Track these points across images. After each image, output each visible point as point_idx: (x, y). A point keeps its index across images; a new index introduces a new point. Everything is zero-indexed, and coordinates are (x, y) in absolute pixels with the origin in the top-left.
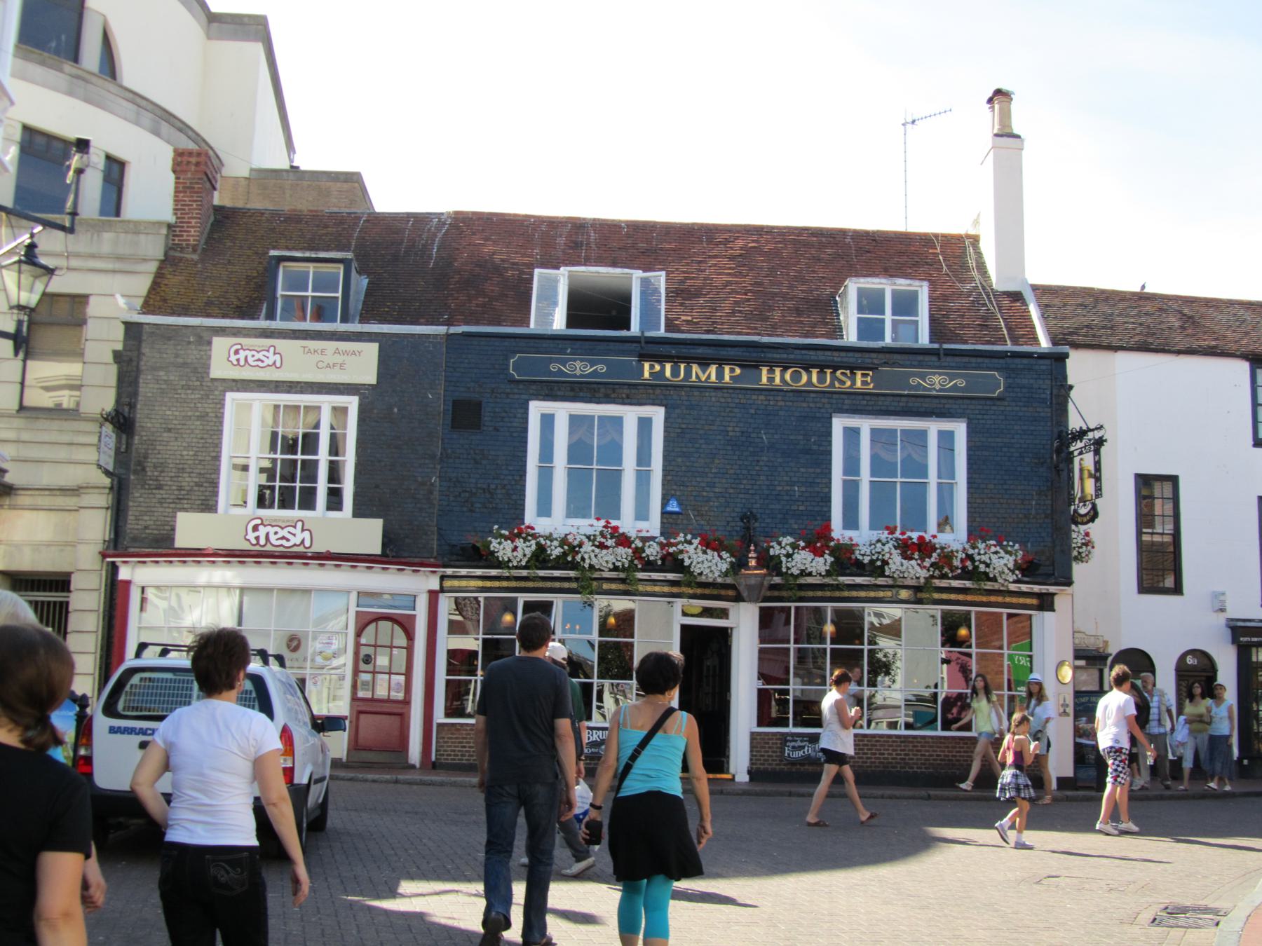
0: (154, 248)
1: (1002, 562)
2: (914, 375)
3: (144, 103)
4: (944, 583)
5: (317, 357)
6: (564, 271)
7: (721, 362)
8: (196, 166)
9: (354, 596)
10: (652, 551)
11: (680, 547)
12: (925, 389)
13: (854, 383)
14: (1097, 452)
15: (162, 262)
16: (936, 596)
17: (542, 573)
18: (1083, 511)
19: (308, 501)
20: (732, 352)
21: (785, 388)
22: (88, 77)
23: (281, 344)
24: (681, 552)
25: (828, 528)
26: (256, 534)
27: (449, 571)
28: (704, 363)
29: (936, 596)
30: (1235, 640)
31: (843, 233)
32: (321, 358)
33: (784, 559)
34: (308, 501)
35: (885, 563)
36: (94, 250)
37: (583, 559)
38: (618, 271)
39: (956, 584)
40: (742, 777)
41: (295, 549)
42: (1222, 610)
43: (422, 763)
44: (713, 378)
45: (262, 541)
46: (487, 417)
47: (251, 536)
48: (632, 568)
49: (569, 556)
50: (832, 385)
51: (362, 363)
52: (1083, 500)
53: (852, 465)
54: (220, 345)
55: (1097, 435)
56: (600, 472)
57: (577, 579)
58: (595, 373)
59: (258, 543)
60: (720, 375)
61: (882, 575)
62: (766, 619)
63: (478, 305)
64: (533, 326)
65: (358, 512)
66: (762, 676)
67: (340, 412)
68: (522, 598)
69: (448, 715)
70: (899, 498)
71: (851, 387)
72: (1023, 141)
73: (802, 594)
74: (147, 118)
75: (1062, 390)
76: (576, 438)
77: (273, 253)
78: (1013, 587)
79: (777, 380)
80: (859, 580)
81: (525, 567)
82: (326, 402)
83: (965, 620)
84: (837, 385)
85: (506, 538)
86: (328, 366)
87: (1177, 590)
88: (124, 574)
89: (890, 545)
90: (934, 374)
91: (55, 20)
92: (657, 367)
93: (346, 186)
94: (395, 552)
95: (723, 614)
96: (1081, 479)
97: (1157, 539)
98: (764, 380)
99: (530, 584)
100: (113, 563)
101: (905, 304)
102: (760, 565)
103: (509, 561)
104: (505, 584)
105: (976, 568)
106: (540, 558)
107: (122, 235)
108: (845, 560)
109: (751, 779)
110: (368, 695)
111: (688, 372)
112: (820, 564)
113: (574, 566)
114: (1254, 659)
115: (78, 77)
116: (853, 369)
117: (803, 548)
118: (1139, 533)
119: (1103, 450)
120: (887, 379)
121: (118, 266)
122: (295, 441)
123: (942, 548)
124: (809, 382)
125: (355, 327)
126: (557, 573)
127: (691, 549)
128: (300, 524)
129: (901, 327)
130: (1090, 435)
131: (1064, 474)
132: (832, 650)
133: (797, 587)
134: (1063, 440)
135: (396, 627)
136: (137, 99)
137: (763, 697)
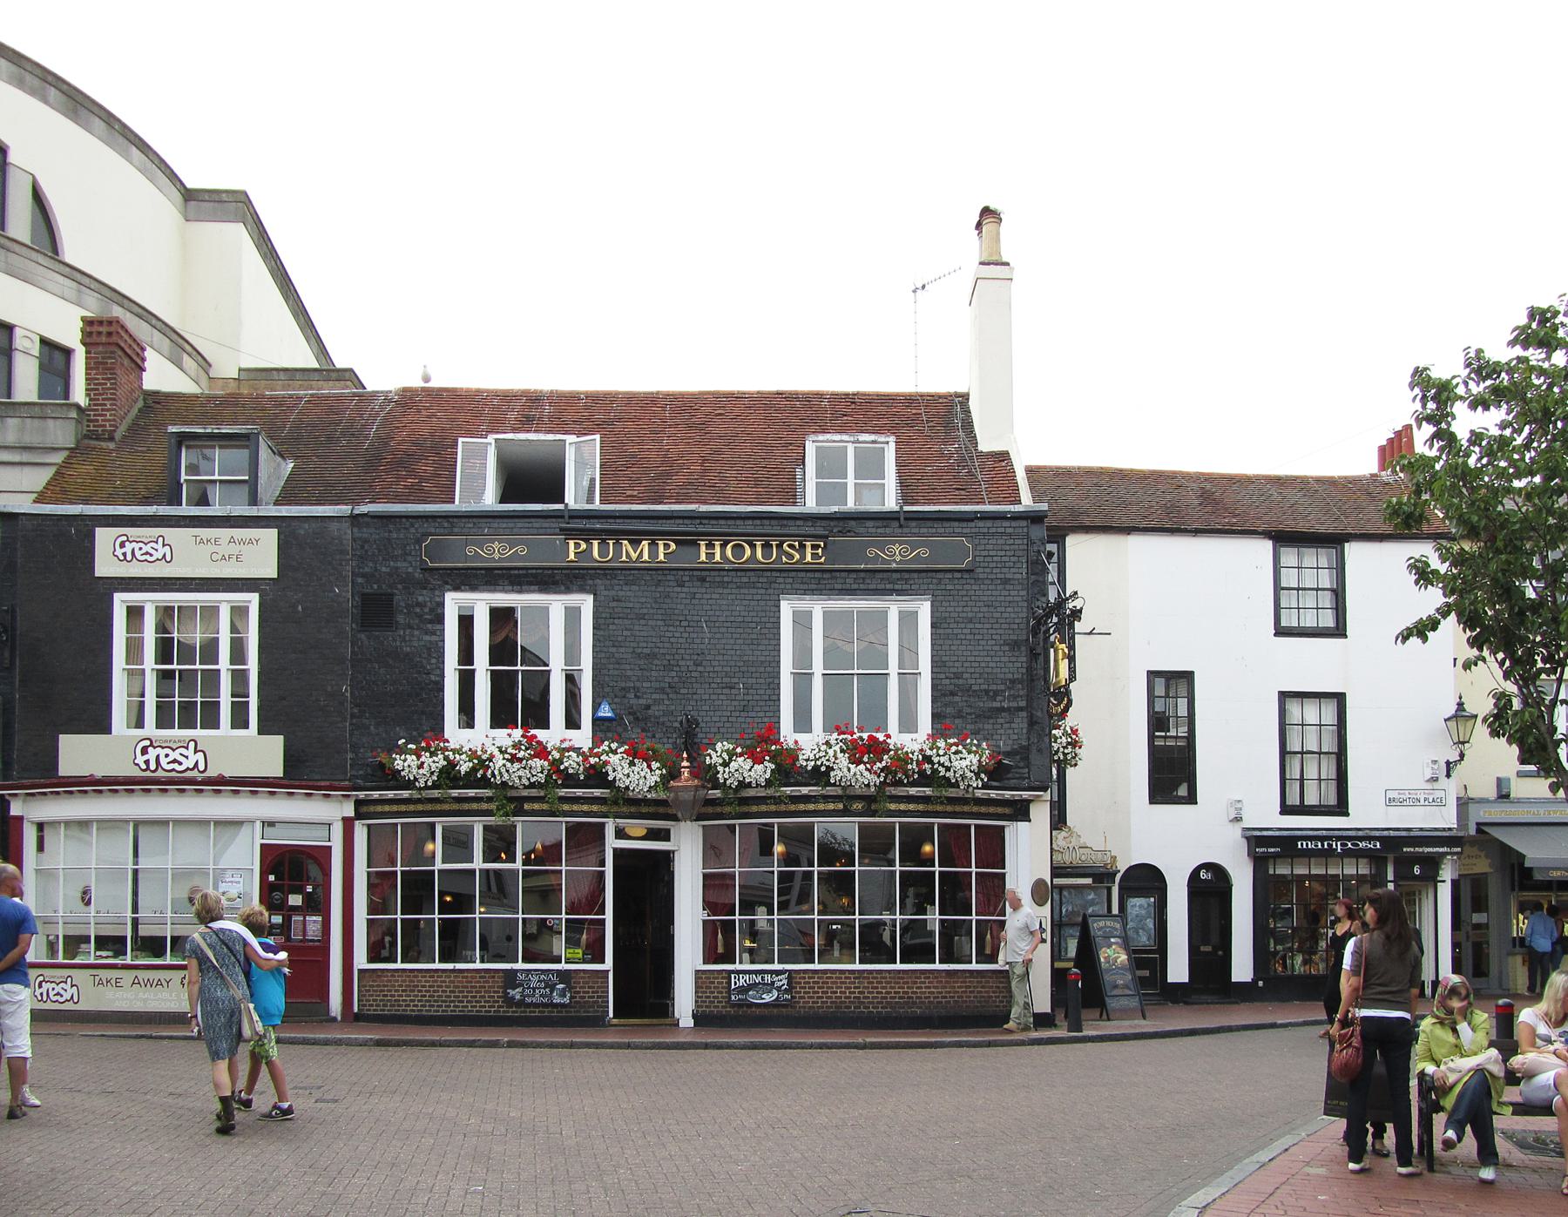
1: (964, 763)
2: (872, 544)
3: (86, 281)
4: (901, 791)
5: (211, 548)
6: (491, 438)
8: (112, 342)
9: (258, 825)
10: (572, 762)
11: (604, 757)
12: (884, 561)
13: (803, 556)
16: (893, 806)
17: (455, 793)
19: (212, 721)
21: (726, 566)
23: (171, 534)
24: (606, 763)
25: (774, 728)
26: (146, 757)
27: (362, 794)
29: (893, 806)
30: (1252, 854)
31: (820, 396)
32: (215, 548)
33: (720, 769)
34: (212, 721)
35: (830, 769)
37: (493, 775)
38: (550, 437)
39: (913, 791)
40: (686, 1021)
41: (189, 774)
42: (1238, 819)
43: (343, 1014)
44: (646, 557)
45: (153, 767)
47: (141, 760)
48: (547, 784)
49: (479, 775)
51: (259, 555)
53: (466, 654)
54: (105, 538)
57: (490, 799)
58: (515, 556)
59: (148, 768)
61: (828, 784)
64: (459, 505)
65: (262, 731)
67: (239, 612)
68: (440, 824)
69: (371, 960)
70: (854, 694)
73: (745, 809)
76: (500, 638)
77: (173, 429)
78: (979, 793)
79: (718, 558)
80: (805, 790)
81: (435, 786)
82: (225, 601)
83: (925, 833)
85: (412, 752)
86: (223, 558)
87: (1191, 799)
88: (16, 809)
89: (837, 748)
92: (584, 546)
94: (300, 774)
95: (664, 835)
97: (1170, 743)
98: (703, 557)
101: (870, 465)
102: (693, 775)
103: (416, 779)
104: (420, 807)
105: (935, 771)
106: (449, 775)
108: (787, 767)
111: (618, 553)
112: (762, 772)
113: (485, 783)
114: (1271, 872)
117: (741, 755)
118: (1151, 738)
120: (845, 554)
121: (26, 457)
123: (897, 750)
126: (471, 793)
127: (614, 759)
128: (192, 744)
129: (865, 492)
132: (780, 873)
133: (741, 799)
137: (709, 929)
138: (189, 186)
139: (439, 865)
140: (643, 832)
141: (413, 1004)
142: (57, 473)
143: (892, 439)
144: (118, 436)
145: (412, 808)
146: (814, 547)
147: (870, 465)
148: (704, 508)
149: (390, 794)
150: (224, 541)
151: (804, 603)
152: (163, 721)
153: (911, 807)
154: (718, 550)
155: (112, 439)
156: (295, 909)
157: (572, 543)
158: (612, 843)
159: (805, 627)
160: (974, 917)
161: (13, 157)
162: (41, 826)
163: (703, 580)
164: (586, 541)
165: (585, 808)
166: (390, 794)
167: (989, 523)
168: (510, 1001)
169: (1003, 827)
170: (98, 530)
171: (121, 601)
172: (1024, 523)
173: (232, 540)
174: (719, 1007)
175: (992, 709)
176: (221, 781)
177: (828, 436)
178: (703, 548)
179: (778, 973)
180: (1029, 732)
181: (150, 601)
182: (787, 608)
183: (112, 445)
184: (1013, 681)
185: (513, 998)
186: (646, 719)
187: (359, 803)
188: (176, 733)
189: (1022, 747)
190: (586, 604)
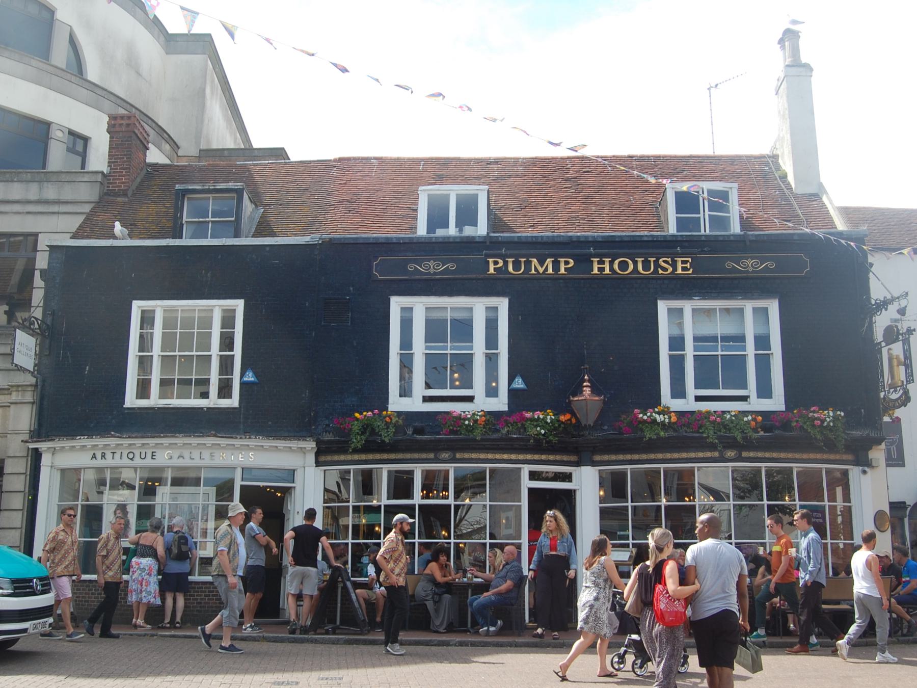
8: (129, 130)
13: (675, 269)
18: (894, 396)
44: (550, 271)
50: (656, 271)
55: (903, 303)
60: (556, 265)
62: (614, 487)
71: (673, 272)
72: (811, 70)
77: (177, 187)
79: (607, 271)
84: (660, 271)
90: (747, 258)
91: (35, 37)
95: (567, 477)
98: (596, 271)
100: (37, 449)
119: (912, 338)
124: (636, 269)
138: (171, 31)
142: (86, 219)
144: (130, 193)
146: (683, 262)
151: (676, 304)
154: (607, 267)
155: (125, 195)
158: (526, 484)
159: (681, 322)
161: (59, 15)
190: (503, 305)
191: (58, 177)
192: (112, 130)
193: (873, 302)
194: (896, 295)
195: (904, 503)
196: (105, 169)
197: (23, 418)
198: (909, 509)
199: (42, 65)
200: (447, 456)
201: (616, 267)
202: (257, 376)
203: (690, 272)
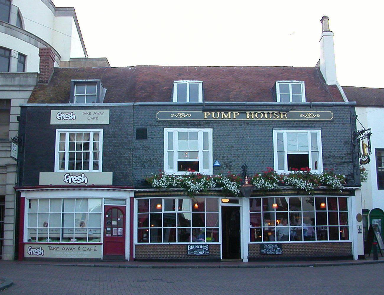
0: (33, 82)
3: (32, 36)
5: (88, 116)
7: (232, 111)
14: (369, 138)
15: (36, 87)
18: (364, 160)
19: (86, 167)
20: (236, 108)
22: (12, 27)
23: (75, 111)
27: (137, 190)
28: (226, 111)
32: (89, 116)
34: (86, 167)
36: (12, 84)
41: (82, 184)
43: (130, 259)
44: (230, 117)
45: (70, 182)
46: (148, 135)
47: (66, 180)
50: (272, 117)
52: (364, 155)
54: (53, 113)
55: (369, 132)
56: (187, 147)
58: (187, 117)
63: (145, 96)
66: (251, 223)
67: (96, 135)
69: (138, 242)
71: (255, 113)
74: (33, 41)
75: (354, 118)
77: (72, 80)
79: (253, 117)
82: (92, 131)
84: (274, 117)
88: (23, 195)
90: (308, 113)
92: (210, 114)
93: (102, 62)
94: (117, 185)
95: (237, 202)
96: (363, 148)
98: (248, 117)
99: (167, 194)
101: (296, 89)
104: (157, 194)
107: (22, 78)
109: (249, 261)
110: (110, 235)
111: (221, 116)
115: (8, 27)
116: (280, 112)
118: (377, 169)
119: (371, 137)
121: (21, 89)
122: (81, 145)
124: (264, 117)
125: (102, 104)
128: (83, 175)
130: (366, 132)
131: (357, 147)
134: (356, 135)
135: (119, 211)
136: (29, 34)
137: (252, 230)
139: (163, 212)
140: (228, 200)
141: (154, 255)
142: (32, 93)
143: (303, 82)
144: (49, 81)
145: (154, 194)
147: (296, 89)
148: (248, 103)
149: (148, 190)
150: (92, 113)
151: (280, 131)
152: (71, 167)
153: (319, 192)
154: (253, 115)
155: (47, 82)
156: (115, 226)
157: (206, 114)
160: (191, 227)
162: (30, 200)
163: (248, 124)
164: (210, 112)
165: (212, 193)
166: (148, 190)
167: (338, 107)
168: (262, 254)
169: (346, 198)
170: (52, 111)
171: (58, 132)
172: (349, 107)
173: (95, 113)
174: (257, 255)
175: (341, 162)
176: (93, 186)
177: (283, 81)
178: (248, 114)
179: (204, 245)
180: (353, 169)
181: (68, 132)
182: (275, 132)
183: (47, 84)
184: (348, 154)
185: (263, 252)
186: (231, 166)
187: (135, 192)
188: (75, 171)
189: (351, 173)
190: (210, 131)
191: (15, 75)
192: (41, 54)
193: (358, 131)
194: (366, 129)
195: (368, 209)
196: (38, 71)
197: (12, 179)
198: (370, 212)
199: (7, 25)
200: (303, 192)
201: (256, 115)
202: (219, 163)
203: (286, 118)
